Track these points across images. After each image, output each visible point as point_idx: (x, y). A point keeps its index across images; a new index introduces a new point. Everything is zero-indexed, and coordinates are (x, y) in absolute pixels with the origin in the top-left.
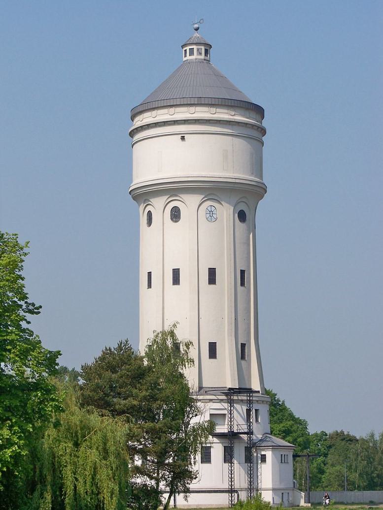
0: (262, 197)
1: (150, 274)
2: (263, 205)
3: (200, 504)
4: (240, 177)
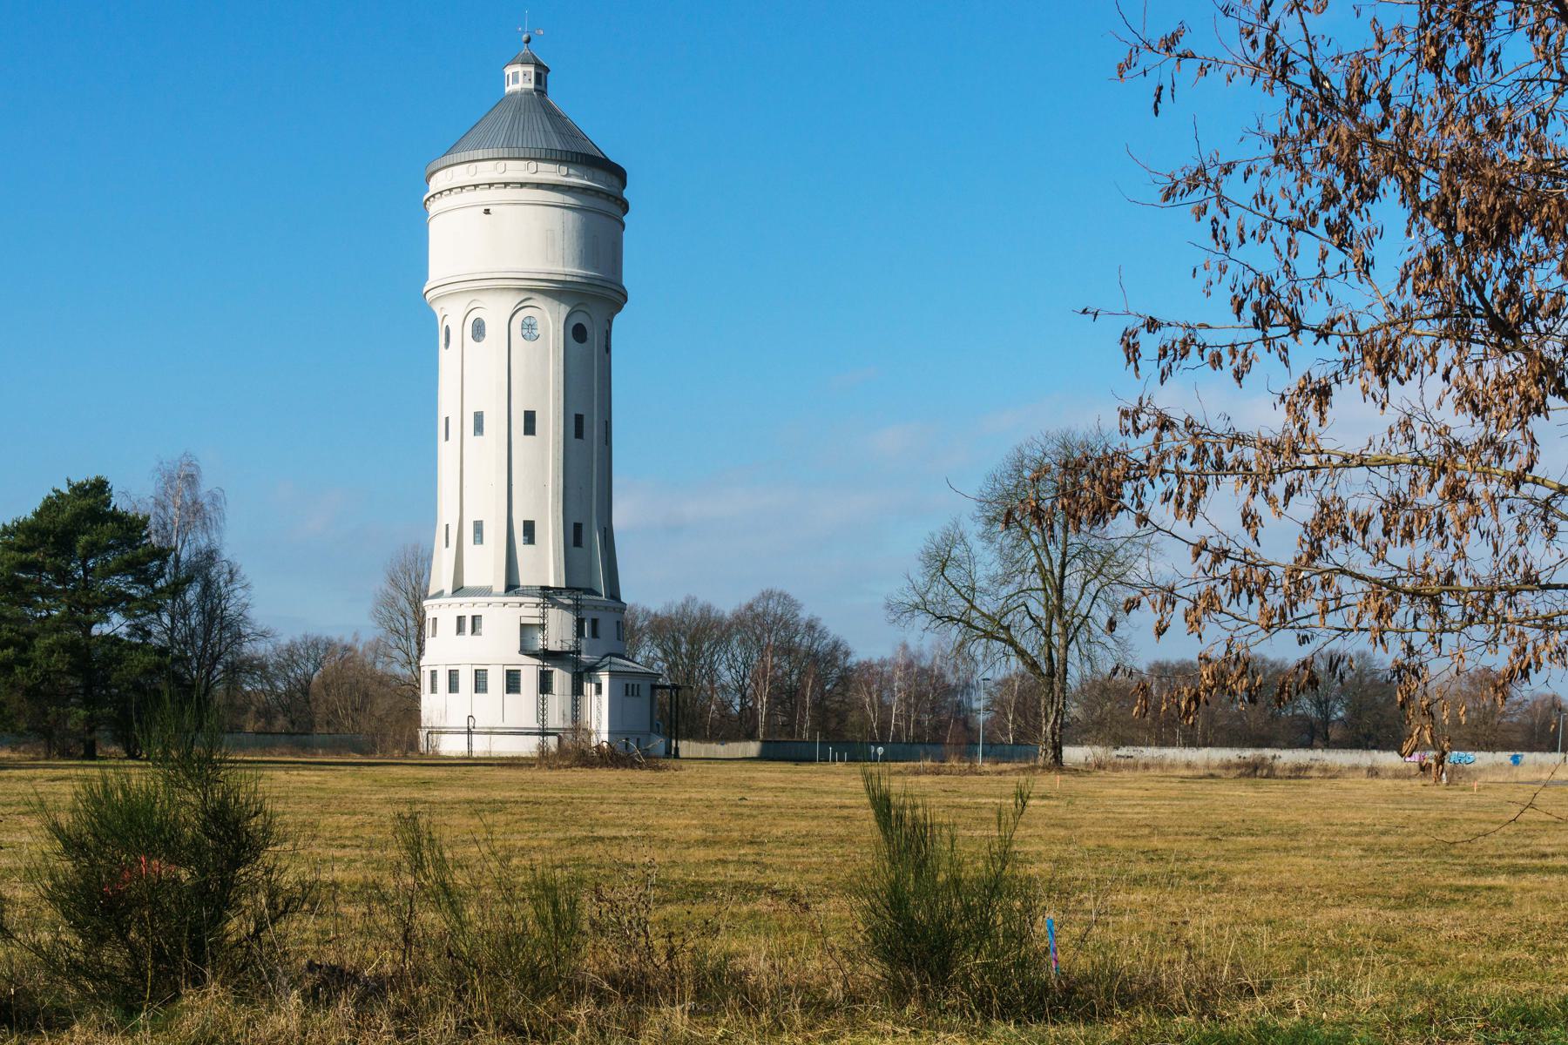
0: (619, 307)
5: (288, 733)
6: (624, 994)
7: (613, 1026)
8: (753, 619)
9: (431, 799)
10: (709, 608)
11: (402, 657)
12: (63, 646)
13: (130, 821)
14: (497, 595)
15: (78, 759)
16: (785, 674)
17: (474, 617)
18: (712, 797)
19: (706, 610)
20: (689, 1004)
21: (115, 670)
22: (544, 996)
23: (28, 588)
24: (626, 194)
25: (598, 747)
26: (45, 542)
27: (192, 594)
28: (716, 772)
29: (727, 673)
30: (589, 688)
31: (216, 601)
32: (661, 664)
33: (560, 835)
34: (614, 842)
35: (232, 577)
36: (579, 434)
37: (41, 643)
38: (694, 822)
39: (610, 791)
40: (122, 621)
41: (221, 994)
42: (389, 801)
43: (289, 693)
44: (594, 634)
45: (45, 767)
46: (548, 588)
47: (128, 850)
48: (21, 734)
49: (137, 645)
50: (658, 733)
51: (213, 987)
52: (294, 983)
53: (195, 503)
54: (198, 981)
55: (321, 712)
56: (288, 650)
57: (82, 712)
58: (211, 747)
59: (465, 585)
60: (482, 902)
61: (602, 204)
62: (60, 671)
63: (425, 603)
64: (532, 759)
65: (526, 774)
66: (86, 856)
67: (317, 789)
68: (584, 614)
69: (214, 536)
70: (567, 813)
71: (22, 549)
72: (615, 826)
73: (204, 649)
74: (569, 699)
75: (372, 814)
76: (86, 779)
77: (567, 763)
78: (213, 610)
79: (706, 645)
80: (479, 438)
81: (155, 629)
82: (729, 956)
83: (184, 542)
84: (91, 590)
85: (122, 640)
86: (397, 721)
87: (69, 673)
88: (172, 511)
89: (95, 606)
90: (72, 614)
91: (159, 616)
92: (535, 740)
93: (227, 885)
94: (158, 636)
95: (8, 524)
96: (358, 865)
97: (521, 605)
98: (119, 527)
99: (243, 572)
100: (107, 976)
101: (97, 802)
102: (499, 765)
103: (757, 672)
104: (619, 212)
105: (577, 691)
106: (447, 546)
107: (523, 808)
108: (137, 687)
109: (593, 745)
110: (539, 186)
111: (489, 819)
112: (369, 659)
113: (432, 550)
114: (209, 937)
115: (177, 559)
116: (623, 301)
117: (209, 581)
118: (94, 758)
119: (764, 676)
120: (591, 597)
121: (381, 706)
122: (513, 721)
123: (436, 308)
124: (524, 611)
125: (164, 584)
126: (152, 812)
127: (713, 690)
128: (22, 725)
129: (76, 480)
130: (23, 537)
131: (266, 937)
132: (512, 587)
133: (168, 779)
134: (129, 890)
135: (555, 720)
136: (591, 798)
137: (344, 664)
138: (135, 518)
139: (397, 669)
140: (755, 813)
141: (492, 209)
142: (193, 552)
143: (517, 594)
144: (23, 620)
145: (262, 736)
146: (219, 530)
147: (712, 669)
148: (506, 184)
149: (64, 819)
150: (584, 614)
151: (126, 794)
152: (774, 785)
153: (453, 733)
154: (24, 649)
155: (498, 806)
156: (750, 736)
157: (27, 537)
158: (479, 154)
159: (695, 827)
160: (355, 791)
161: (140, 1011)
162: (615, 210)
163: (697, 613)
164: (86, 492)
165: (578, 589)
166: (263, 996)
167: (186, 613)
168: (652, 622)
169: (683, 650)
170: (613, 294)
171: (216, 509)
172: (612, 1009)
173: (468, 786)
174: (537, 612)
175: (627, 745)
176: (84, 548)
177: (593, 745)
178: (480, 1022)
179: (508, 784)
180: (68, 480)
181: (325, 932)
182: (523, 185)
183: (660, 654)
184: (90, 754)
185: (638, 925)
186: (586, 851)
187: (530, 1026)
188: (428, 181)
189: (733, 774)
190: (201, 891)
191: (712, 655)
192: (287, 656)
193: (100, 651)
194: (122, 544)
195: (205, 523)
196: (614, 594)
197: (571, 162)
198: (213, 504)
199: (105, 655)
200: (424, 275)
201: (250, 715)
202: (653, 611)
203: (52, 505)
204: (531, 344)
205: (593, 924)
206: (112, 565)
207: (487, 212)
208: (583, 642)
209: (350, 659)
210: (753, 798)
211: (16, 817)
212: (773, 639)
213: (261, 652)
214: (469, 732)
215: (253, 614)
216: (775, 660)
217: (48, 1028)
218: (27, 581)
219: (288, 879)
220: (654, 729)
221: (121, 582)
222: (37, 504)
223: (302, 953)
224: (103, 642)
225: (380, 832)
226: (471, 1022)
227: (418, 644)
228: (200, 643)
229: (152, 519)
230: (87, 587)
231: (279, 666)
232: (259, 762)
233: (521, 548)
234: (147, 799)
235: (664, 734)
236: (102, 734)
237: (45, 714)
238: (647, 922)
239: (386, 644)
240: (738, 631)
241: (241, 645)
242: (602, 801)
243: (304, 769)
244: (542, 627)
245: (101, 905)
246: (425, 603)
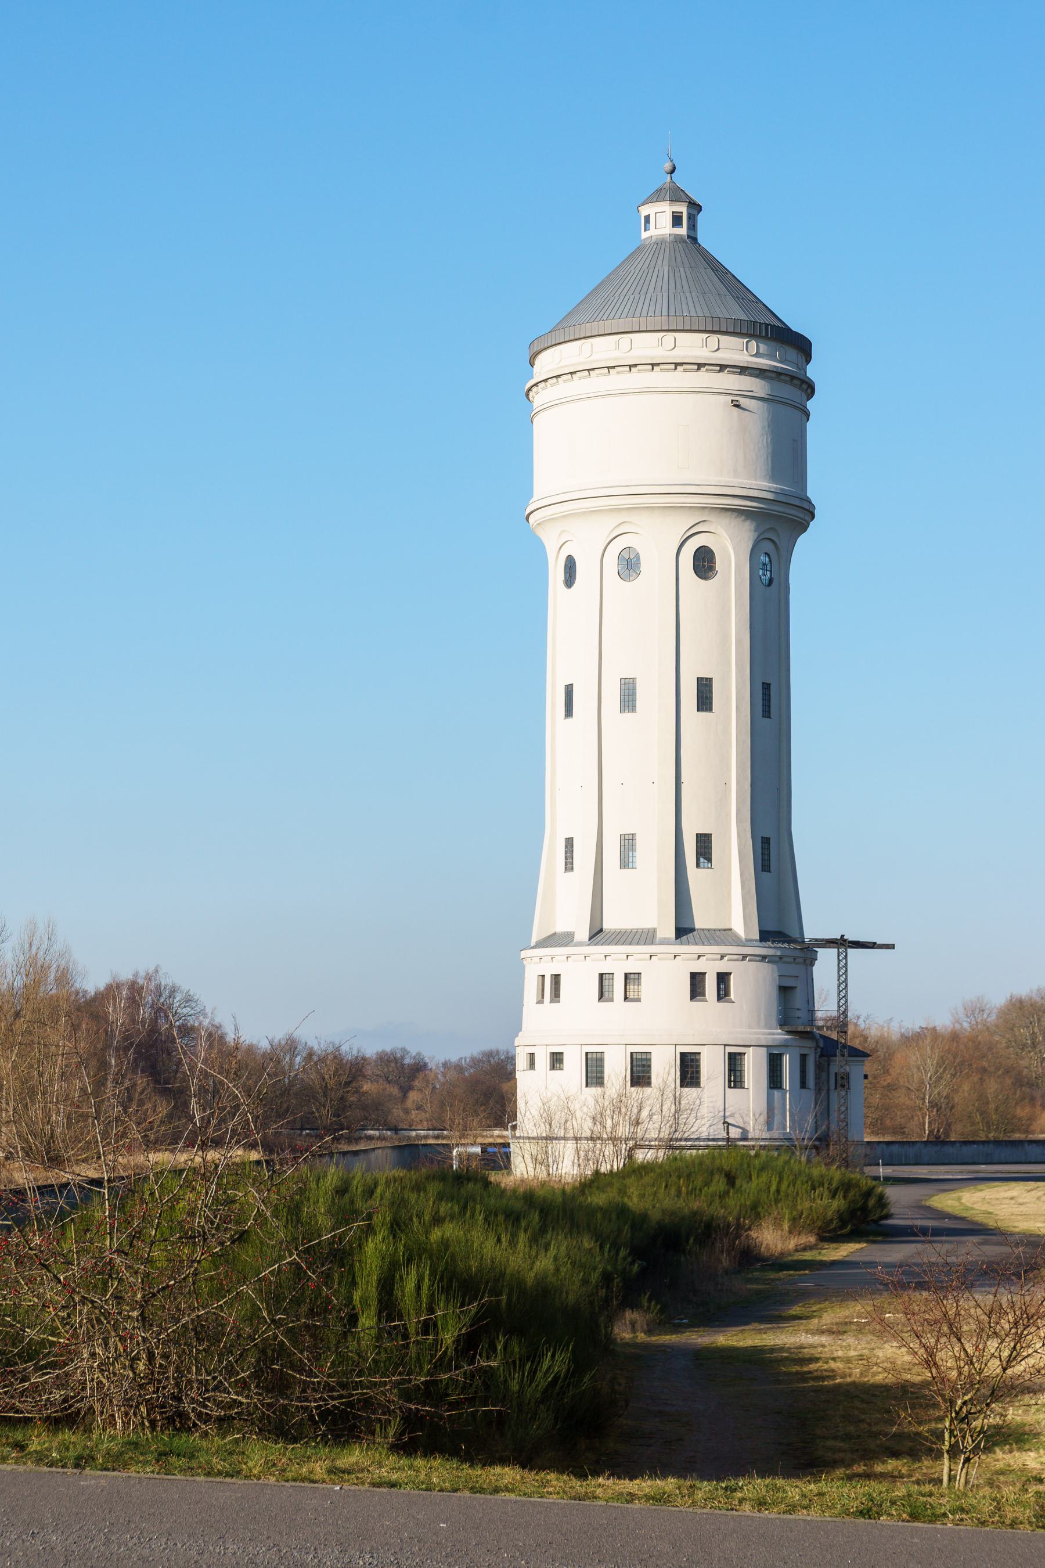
0: (803, 527)
1: (569, 690)
2: (804, 545)
14: (664, 942)
59: (605, 927)
110: (743, 370)
132: (683, 931)
148: (722, 368)
188: (532, 365)
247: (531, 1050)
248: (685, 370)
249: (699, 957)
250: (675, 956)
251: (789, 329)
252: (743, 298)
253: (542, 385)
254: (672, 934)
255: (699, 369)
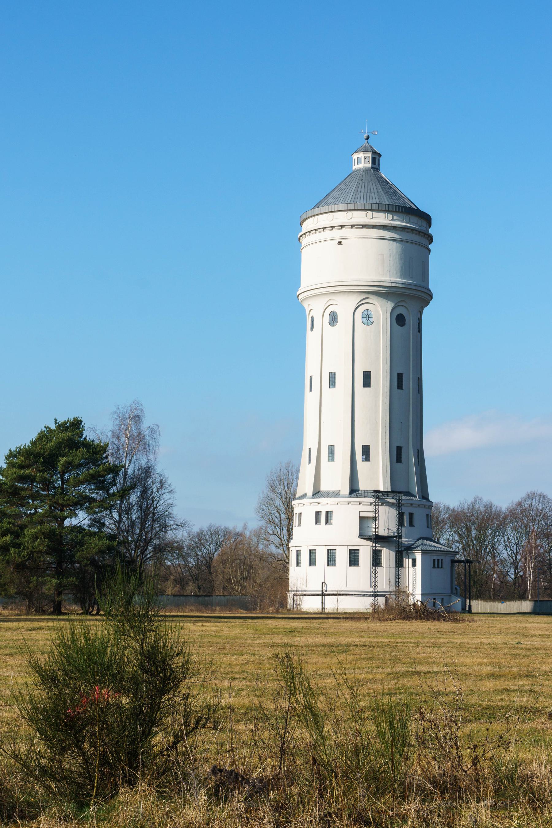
0: (427, 303)
3: (346, 607)
4: (397, 281)
5: (196, 596)
6: (442, 792)
7: (436, 818)
8: (522, 513)
9: (296, 643)
10: (491, 505)
11: (277, 540)
12: (44, 533)
13: (90, 659)
15: (49, 615)
16: (545, 551)
17: (327, 512)
18: (497, 642)
19: (489, 507)
20: (490, 802)
21: (79, 551)
22: (383, 794)
23: (23, 493)
24: (431, 231)
25: (414, 605)
26: (37, 462)
27: (134, 498)
28: (499, 623)
29: (504, 551)
30: (407, 562)
31: (150, 502)
32: (457, 544)
33: (388, 670)
34: (428, 675)
35: (162, 485)
36: (400, 386)
37: (29, 532)
38: (485, 660)
39: (423, 638)
40: (86, 516)
41: (147, 792)
42: (265, 645)
43: (198, 567)
44: (411, 524)
45: (26, 620)
46: (378, 492)
47: (86, 681)
48: (11, 597)
49: (95, 533)
50: (456, 595)
51: (141, 786)
52: (203, 783)
53: (139, 434)
54: (132, 782)
55: (219, 580)
56: (198, 536)
57: (54, 581)
58: (149, 605)
59: (321, 490)
60: (337, 722)
61: (416, 238)
62: (40, 552)
63: (294, 502)
64: (367, 614)
65: (363, 625)
66: (57, 686)
67: (216, 636)
68: (404, 509)
69: (151, 457)
70: (393, 654)
71: (21, 467)
72: (427, 663)
73: (140, 536)
74: (393, 570)
75: (254, 655)
76: (61, 629)
77: (392, 617)
78: (148, 508)
79: (489, 532)
80: (332, 389)
81: (107, 522)
82: (517, 764)
83: (130, 461)
84: (66, 494)
85: (84, 529)
86: (272, 587)
87: (47, 553)
88: (124, 440)
89: (68, 505)
90: (52, 511)
91: (111, 512)
92: (369, 600)
93: (155, 707)
94: (110, 528)
95: (13, 449)
96: (244, 693)
97: (360, 503)
98: (88, 452)
99: (169, 481)
100: (65, 778)
101: (64, 645)
102: (344, 618)
103: (525, 550)
104: (427, 242)
105: (399, 564)
106: (309, 463)
107: (361, 650)
108: (94, 563)
109: (410, 603)
110: (374, 227)
111: (342, 657)
112: (253, 542)
113: (299, 466)
114: (142, 747)
115: (126, 473)
116: (429, 298)
117: (146, 488)
118: (60, 613)
119: (531, 553)
120: (408, 498)
121: (261, 575)
122: (354, 587)
123: (305, 305)
124: (362, 508)
125: (115, 490)
126: (105, 654)
127: (495, 563)
128: (12, 590)
129: (61, 420)
130: (23, 458)
131: (180, 747)
132: (354, 491)
133: (117, 631)
134: (85, 712)
135: (383, 586)
136: (410, 643)
137: (236, 546)
138: (98, 445)
139: (273, 549)
140: (528, 653)
141: (343, 241)
142: (136, 469)
143: (357, 496)
144: (18, 516)
145: (177, 598)
146: (154, 452)
147: (494, 549)
148: (353, 226)
149: (42, 659)
150: (404, 509)
151: (87, 640)
152: (540, 633)
153: (311, 595)
154: (17, 536)
155: (346, 648)
156: (522, 597)
157: (25, 459)
158: (335, 207)
159: (486, 664)
160: (242, 638)
161: (88, 805)
162: (424, 241)
163: (482, 509)
164: (67, 428)
165: (400, 492)
166: (179, 794)
167: (129, 510)
168: (450, 516)
169: (473, 535)
170: (423, 295)
171: (153, 439)
172: (435, 805)
173: (322, 634)
174: (371, 508)
175: (434, 603)
176: (63, 466)
177: (410, 603)
178: (336, 814)
179: (351, 632)
180: (56, 420)
181: (222, 744)
182: (363, 226)
183: (457, 538)
184: (57, 611)
185: (451, 739)
186: (407, 682)
187: (374, 820)
188: (301, 224)
189: (511, 625)
190: (137, 713)
191: (494, 538)
192: (197, 540)
193: (69, 537)
194: (88, 463)
195: (145, 448)
196: (425, 496)
197: (395, 211)
198: (151, 435)
199: (72, 540)
200: (297, 283)
201: (169, 583)
202: (451, 507)
203: (43, 437)
204: (368, 327)
205: (417, 737)
206: (81, 477)
207: (340, 243)
208: (403, 529)
209: (240, 543)
210: (527, 642)
211: (3, 657)
212: (536, 527)
213: (179, 537)
214: (323, 594)
215: (174, 511)
216: (538, 541)
217: (22, 818)
218: (23, 489)
219: (196, 704)
220: (453, 592)
221: (86, 489)
222: (33, 436)
223: (207, 760)
224: (72, 530)
225: (260, 669)
226: (330, 814)
227: (288, 531)
228: (138, 531)
229: (110, 446)
230: (63, 492)
231: (191, 547)
232: (181, 616)
233: (361, 464)
234: (102, 643)
235: (461, 595)
236: (67, 597)
237: (29, 582)
238: (457, 737)
239: (266, 532)
240: (512, 522)
241: (166, 532)
242: (418, 645)
243: (206, 622)
244: (375, 519)
245: (65, 723)
246: (294, 502)
247: (298, 548)
248: (346, 228)
249: (348, 503)
250: (348, 503)
251: (419, 210)
252: (399, 196)
253: (304, 236)
254: (347, 492)
255: (352, 228)
